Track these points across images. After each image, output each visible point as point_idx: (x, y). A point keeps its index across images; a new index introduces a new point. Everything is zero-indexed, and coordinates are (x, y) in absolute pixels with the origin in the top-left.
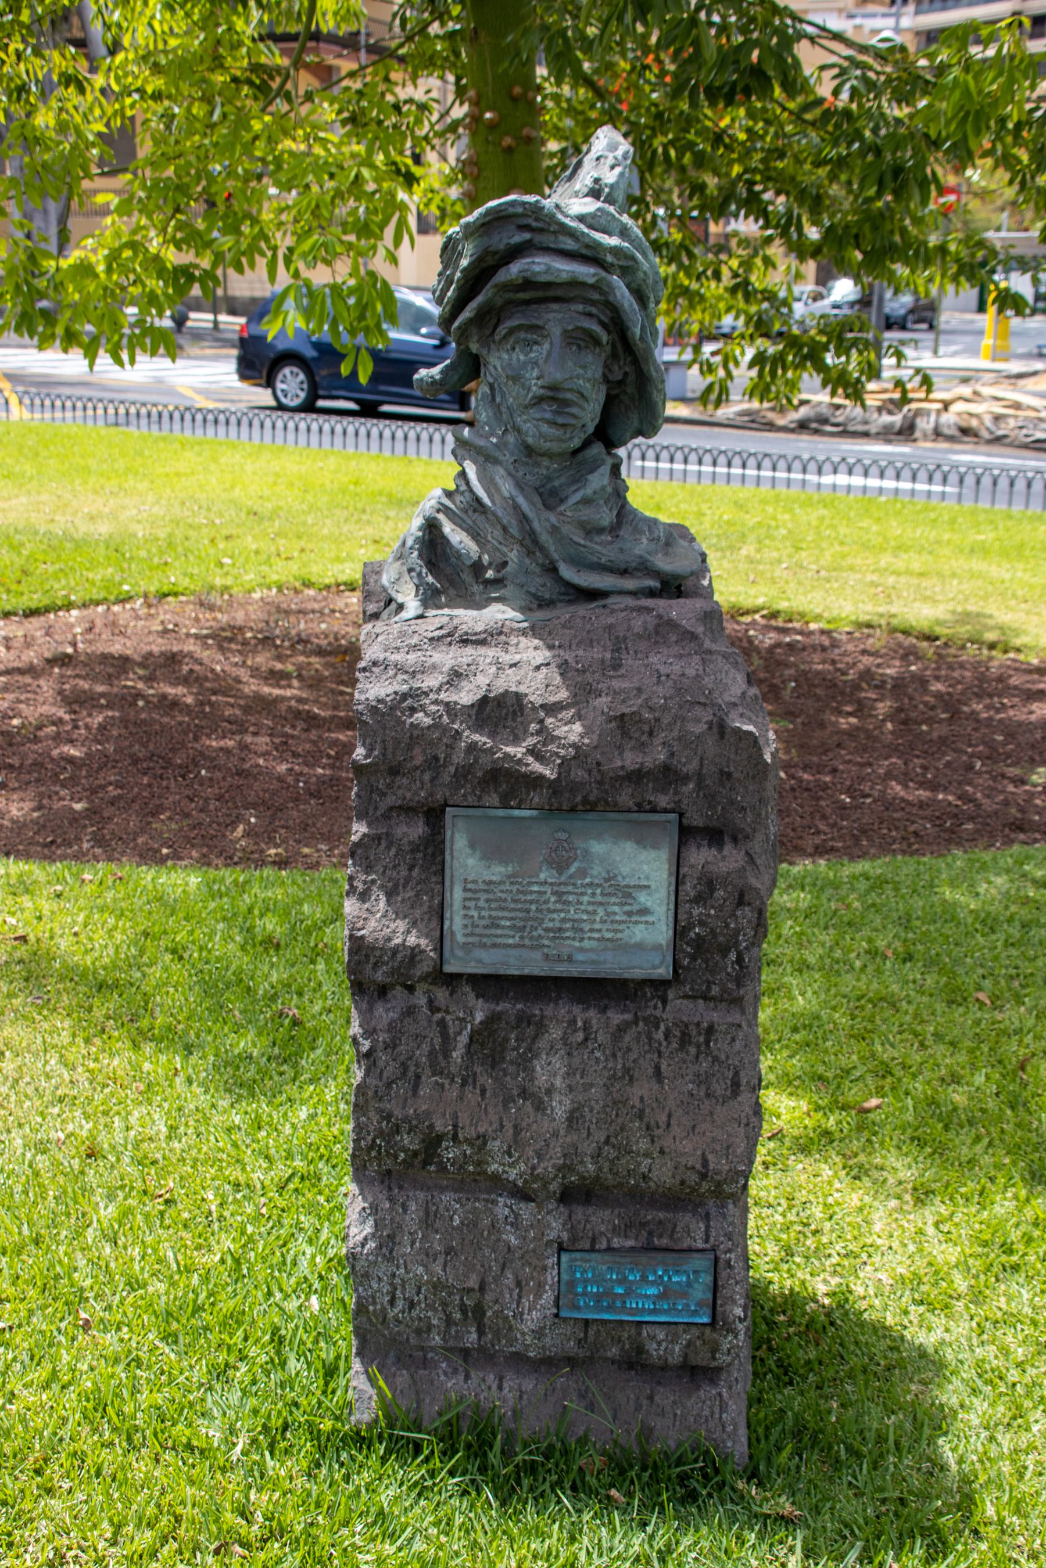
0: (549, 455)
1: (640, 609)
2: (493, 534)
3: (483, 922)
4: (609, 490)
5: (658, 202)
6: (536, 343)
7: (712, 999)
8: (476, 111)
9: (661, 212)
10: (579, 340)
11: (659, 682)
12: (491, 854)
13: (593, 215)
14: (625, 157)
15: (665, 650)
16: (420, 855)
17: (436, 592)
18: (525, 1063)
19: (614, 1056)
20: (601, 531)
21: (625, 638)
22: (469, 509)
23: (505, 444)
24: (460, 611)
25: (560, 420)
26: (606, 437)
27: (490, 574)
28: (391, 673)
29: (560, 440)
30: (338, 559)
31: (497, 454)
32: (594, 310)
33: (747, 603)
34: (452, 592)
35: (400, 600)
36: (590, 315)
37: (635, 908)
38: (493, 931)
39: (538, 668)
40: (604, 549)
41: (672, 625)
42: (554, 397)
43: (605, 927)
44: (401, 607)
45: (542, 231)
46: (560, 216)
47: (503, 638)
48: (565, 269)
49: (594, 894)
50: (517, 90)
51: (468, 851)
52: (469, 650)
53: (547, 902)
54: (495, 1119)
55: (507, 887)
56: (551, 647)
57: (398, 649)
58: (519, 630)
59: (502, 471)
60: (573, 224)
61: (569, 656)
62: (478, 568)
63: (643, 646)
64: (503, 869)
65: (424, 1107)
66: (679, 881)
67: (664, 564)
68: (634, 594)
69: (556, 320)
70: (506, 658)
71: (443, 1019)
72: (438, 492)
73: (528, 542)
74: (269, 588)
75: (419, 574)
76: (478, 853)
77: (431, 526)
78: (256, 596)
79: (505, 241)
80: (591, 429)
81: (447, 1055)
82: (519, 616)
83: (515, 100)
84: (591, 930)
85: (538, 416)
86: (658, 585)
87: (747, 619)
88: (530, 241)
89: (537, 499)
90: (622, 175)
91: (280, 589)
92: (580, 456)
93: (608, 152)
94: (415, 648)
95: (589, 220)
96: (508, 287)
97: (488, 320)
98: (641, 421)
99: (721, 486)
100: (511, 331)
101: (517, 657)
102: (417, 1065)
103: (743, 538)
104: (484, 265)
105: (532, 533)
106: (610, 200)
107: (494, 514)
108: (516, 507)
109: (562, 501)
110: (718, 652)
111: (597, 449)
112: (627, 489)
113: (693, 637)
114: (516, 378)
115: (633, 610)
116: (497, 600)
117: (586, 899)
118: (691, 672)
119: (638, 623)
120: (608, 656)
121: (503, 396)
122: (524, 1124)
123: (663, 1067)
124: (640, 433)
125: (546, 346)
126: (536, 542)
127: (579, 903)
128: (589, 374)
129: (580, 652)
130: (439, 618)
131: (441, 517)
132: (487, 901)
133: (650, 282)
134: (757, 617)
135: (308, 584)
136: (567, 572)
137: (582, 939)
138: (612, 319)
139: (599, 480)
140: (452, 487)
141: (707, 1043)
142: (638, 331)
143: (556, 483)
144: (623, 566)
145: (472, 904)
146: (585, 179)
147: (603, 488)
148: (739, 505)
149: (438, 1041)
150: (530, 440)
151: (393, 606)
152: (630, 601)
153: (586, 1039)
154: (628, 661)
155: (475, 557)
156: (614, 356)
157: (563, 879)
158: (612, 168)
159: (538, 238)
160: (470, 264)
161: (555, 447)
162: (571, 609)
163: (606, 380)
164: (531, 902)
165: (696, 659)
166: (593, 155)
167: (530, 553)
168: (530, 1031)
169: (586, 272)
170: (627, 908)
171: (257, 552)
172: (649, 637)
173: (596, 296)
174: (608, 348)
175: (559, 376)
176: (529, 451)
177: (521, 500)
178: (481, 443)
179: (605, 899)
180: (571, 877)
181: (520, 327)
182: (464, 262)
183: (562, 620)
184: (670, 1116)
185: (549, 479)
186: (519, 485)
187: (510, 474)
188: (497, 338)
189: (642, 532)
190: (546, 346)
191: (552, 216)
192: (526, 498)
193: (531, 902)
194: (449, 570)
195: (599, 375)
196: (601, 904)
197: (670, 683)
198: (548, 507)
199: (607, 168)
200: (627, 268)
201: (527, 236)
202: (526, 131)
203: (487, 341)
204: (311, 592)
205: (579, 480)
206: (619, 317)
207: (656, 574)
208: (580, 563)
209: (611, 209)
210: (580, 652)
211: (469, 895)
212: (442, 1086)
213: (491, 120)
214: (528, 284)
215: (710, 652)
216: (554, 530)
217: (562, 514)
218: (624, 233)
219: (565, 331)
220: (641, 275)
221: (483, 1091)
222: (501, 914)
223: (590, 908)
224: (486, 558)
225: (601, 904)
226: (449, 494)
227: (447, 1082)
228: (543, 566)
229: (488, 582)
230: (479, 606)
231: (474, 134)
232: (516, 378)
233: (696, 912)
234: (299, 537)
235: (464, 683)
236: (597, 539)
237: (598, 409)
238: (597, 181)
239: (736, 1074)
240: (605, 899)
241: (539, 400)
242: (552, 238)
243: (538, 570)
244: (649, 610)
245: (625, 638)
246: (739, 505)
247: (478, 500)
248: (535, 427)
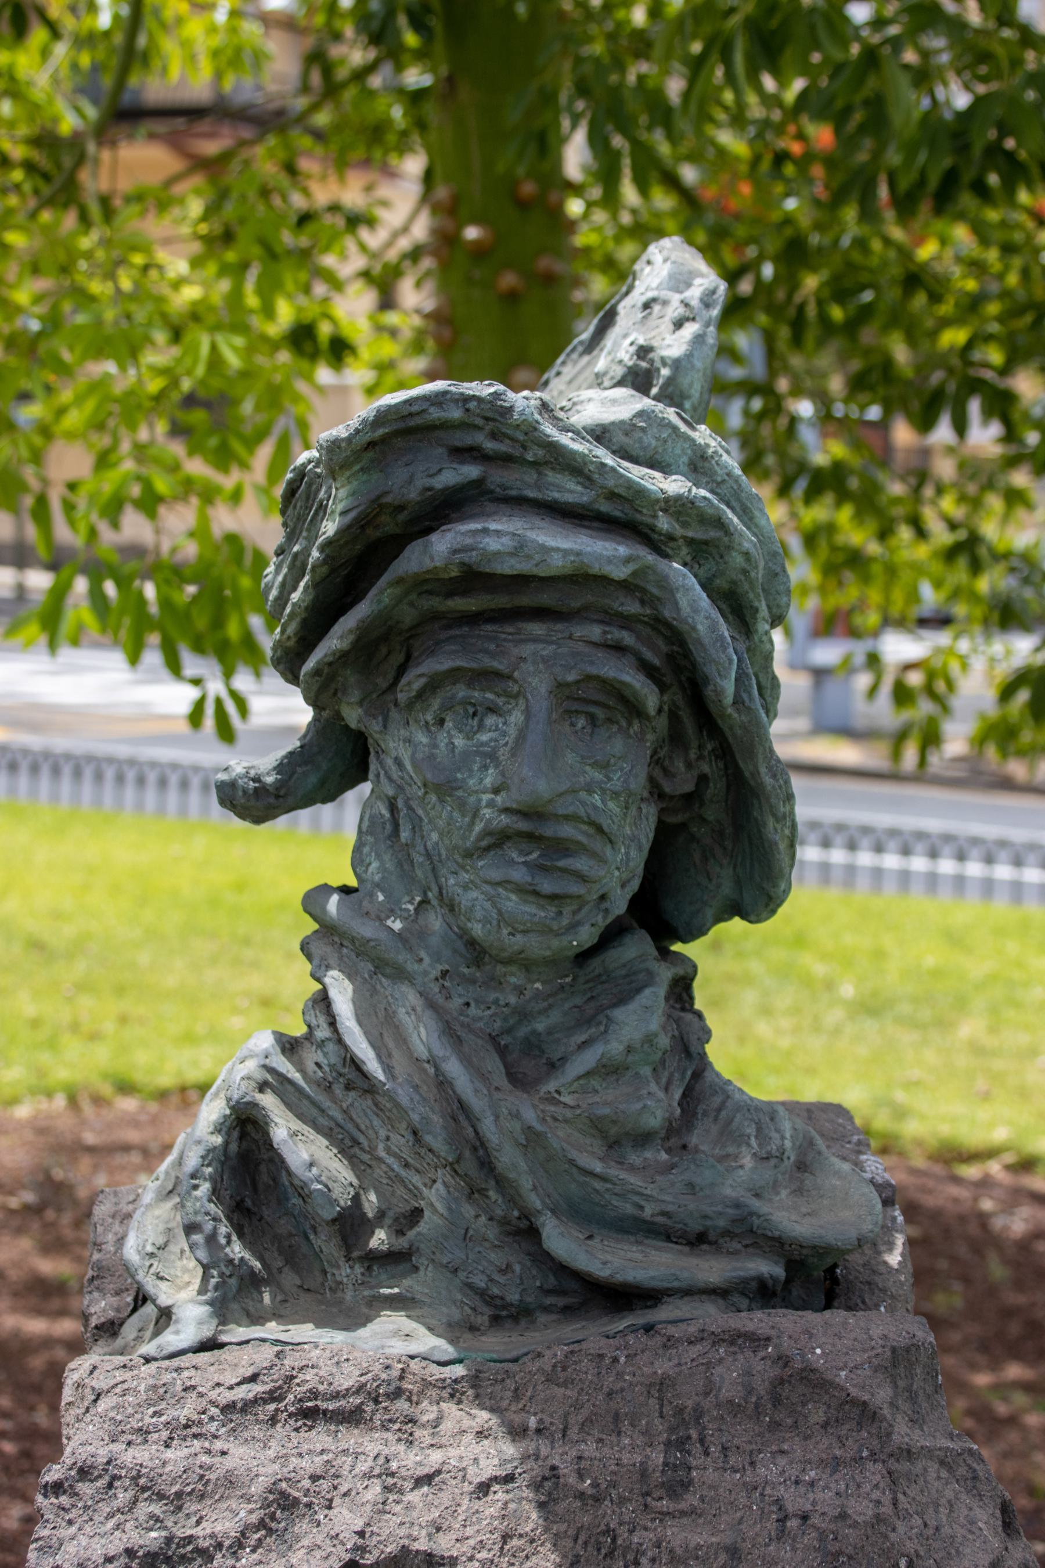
0: (527, 964)
1: (736, 1339)
2: (389, 1144)
4: (664, 1041)
5: (797, 392)
6: (492, 710)
8: (449, 225)
9: (805, 408)
10: (592, 704)
11: (782, 1534)
13: (627, 427)
14: (707, 302)
15: (795, 1445)
17: (252, 1282)
20: (643, 1139)
21: (699, 1413)
22: (330, 1082)
23: (423, 935)
24: (304, 1332)
25: (547, 886)
26: (661, 912)
27: (380, 1239)
28: (123, 1497)
29: (546, 930)
30: (189, 1038)
31: (402, 957)
32: (627, 638)
33: (973, 1137)
34: (290, 1279)
35: (164, 1301)
36: (618, 648)
39: (484, 1489)
40: (646, 1183)
41: (814, 1381)
42: (533, 834)
44: (165, 1316)
45: (504, 462)
46: (549, 429)
47: (402, 1405)
48: (559, 545)
50: (528, 188)
52: (320, 1438)
56: (517, 1432)
57: (143, 1432)
58: (441, 1384)
59: (412, 997)
60: (578, 447)
61: (561, 1456)
62: (351, 1224)
63: (742, 1433)
67: (792, 1219)
68: (719, 1293)
69: (540, 660)
70: (410, 1460)
72: (264, 1041)
73: (469, 1166)
74: (49, 1094)
75: (211, 1239)
77: (245, 1125)
78: (23, 1112)
79: (421, 482)
80: (620, 906)
82: (443, 1348)
83: (523, 205)
85: (495, 875)
86: (778, 1271)
87: (971, 1172)
88: (478, 484)
89: (493, 1064)
90: (698, 339)
91: (73, 1101)
92: (595, 964)
93: (667, 294)
94: (189, 1430)
95: (619, 438)
96: (426, 584)
97: (381, 655)
98: (738, 883)
99: (918, 902)
100: (434, 684)
101: (436, 1457)
103: (961, 1004)
104: (373, 534)
105: (479, 1147)
106: (671, 396)
107: (390, 1096)
108: (443, 1083)
109: (553, 1066)
110: (928, 1453)
111: (637, 947)
112: (706, 1034)
113: (866, 1414)
114: (445, 789)
115: (717, 1339)
116: (396, 1303)
118: (862, 1510)
119: (730, 1375)
120: (657, 1457)
121: (416, 827)
124: (737, 909)
125: (516, 717)
126: (487, 1165)
128: (616, 782)
129: (589, 1448)
130: (262, 1344)
131: (268, 1101)
133: (759, 574)
134: (994, 1168)
135: (125, 1088)
136: (561, 1241)
138: (670, 657)
139: (640, 1020)
140: (298, 1029)
142: (729, 687)
143: (540, 1026)
144: (695, 1226)
146: (619, 348)
147: (649, 1040)
148: (954, 939)
150: (477, 930)
151: (149, 1310)
152: (712, 1316)
154: (706, 1472)
155: (343, 1197)
156: (675, 738)
158: (678, 324)
159: (499, 477)
160: (340, 532)
161: (536, 946)
162: (571, 1330)
163: (656, 792)
165: (874, 1472)
166: (639, 294)
167: (474, 1192)
169: (608, 553)
171: (35, 1023)
172: (758, 1411)
173: (632, 607)
174: (662, 723)
175: (543, 787)
176: (476, 952)
177: (453, 1068)
178: (366, 930)
181: (454, 675)
182: (329, 528)
183: (546, 1363)
185: (523, 1015)
186: (451, 1032)
187: (431, 1005)
188: (402, 697)
189: (742, 1140)
190: (516, 717)
191: (532, 428)
192: (466, 1061)
194: (284, 1226)
195: (639, 783)
197: (810, 1538)
198: (517, 1080)
199: (666, 325)
200: (704, 541)
201: (472, 471)
202: (544, 263)
203: (380, 701)
204: (128, 1104)
205: (593, 1017)
206: (687, 654)
207: (776, 1244)
208: (594, 1217)
209: (670, 414)
210: (589, 1448)
213: (476, 243)
214: (472, 578)
215: (908, 1453)
216: (532, 1140)
217: (551, 1099)
218: (699, 465)
219: (560, 685)
220: (738, 560)
224: (371, 1200)
226: (289, 1046)
228: (504, 1222)
229: (374, 1259)
230: (352, 1319)
231: (445, 266)
232: (445, 789)
234: (120, 990)
235: (302, 1526)
236: (634, 1158)
237: (638, 860)
238: (643, 352)
241: (498, 840)
242: (531, 476)
243: (492, 1232)
244: (756, 1341)
245: (699, 1413)
246: (954, 939)
247: (355, 1064)
248: (489, 900)
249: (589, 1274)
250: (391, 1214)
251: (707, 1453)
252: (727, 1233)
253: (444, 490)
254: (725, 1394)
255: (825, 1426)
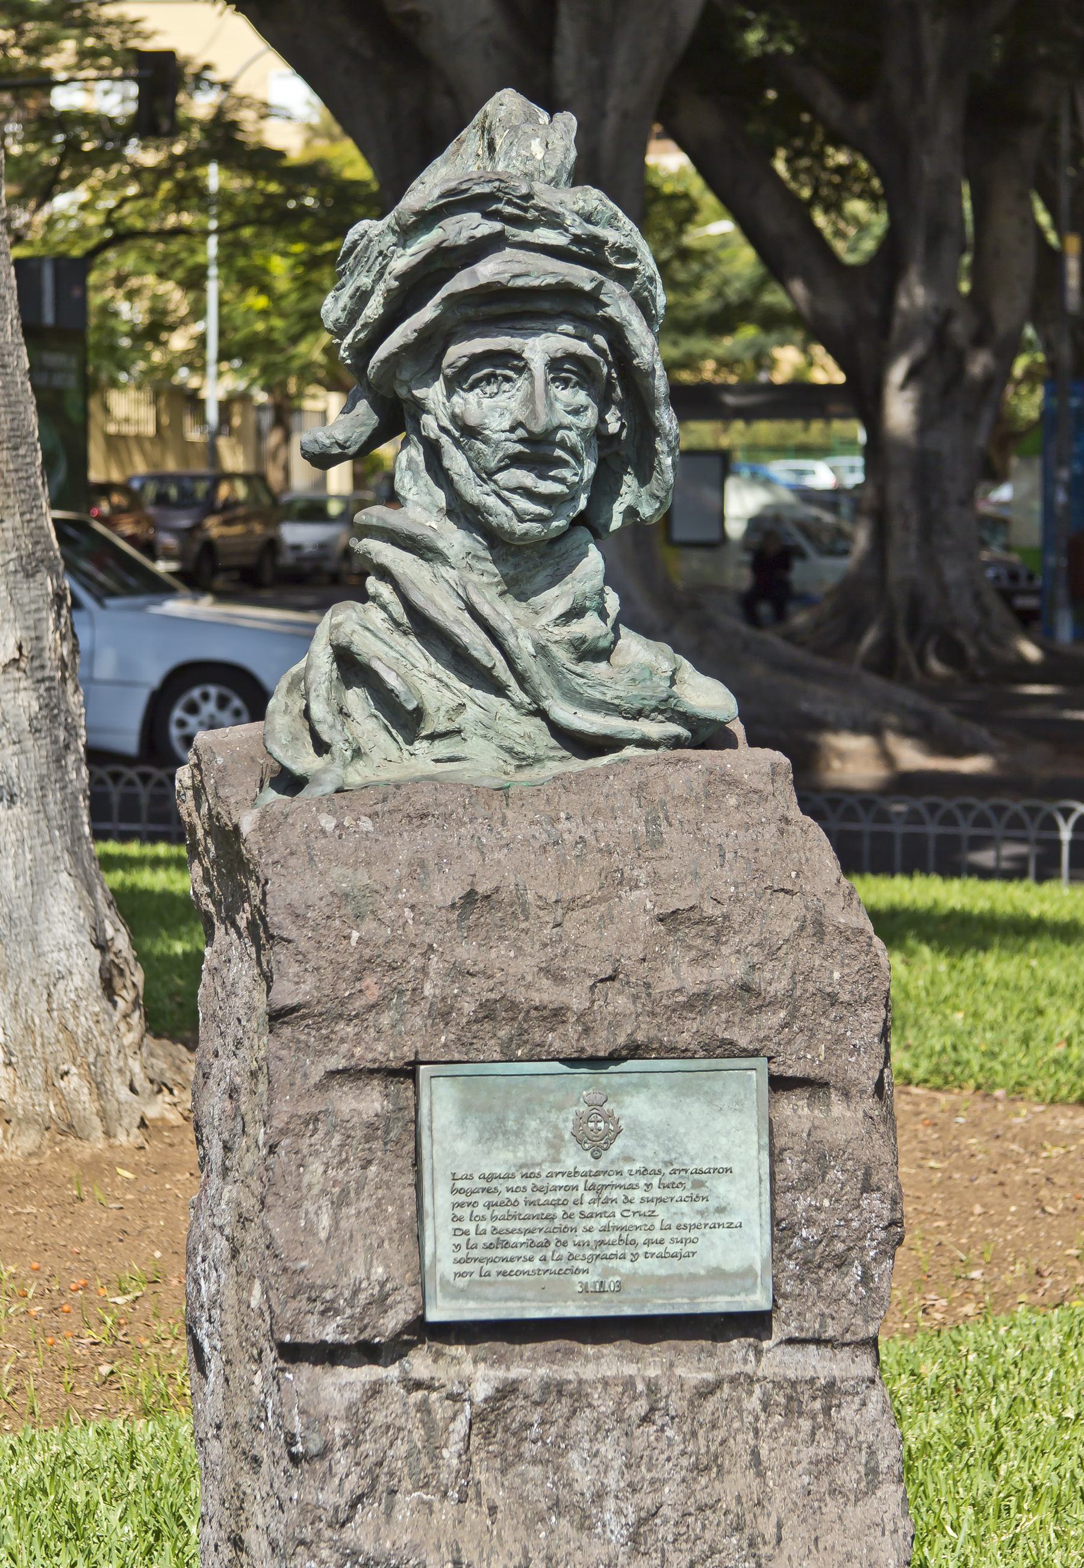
3: (488, 1239)
7: (827, 1342)
12: (495, 1131)
16: (376, 1145)
18: (553, 1459)
19: (694, 1434)
29: (539, 519)
37: (713, 1203)
38: (500, 1253)
43: (668, 1235)
49: (649, 1186)
51: (456, 1129)
53: (578, 1202)
54: (516, 1548)
55: (518, 1182)
64: (510, 1156)
65: (406, 1538)
66: (775, 1156)
71: (425, 1401)
76: (473, 1134)
81: (434, 1456)
84: (648, 1242)
102: (391, 1474)
115: (668, 763)
117: (637, 1194)
122: (560, 1554)
123: (764, 1452)
127: (628, 1200)
132: (489, 1206)
137: (635, 1257)
141: (827, 1410)
144: (637, 705)
145: (465, 1212)
149: (418, 1434)
153: (653, 1409)
157: (601, 1165)
164: (555, 1204)
168: (563, 1408)
170: (700, 1205)
179: (665, 1193)
180: (612, 1162)
184: (779, 1526)
193: (555, 1204)
196: (661, 1200)
211: (462, 1198)
212: (429, 1505)
221: (493, 1510)
222: (511, 1225)
223: (645, 1208)
225: (661, 1200)
227: (435, 1499)
233: (801, 1206)
239: (872, 1454)
240: (665, 1193)
245: (663, 804)
249: (581, 733)
250: (443, 709)
251: (671, 825)
252: (655, 709)
253: (653, 387)
254: (676, 792)
255: (737, 807)
